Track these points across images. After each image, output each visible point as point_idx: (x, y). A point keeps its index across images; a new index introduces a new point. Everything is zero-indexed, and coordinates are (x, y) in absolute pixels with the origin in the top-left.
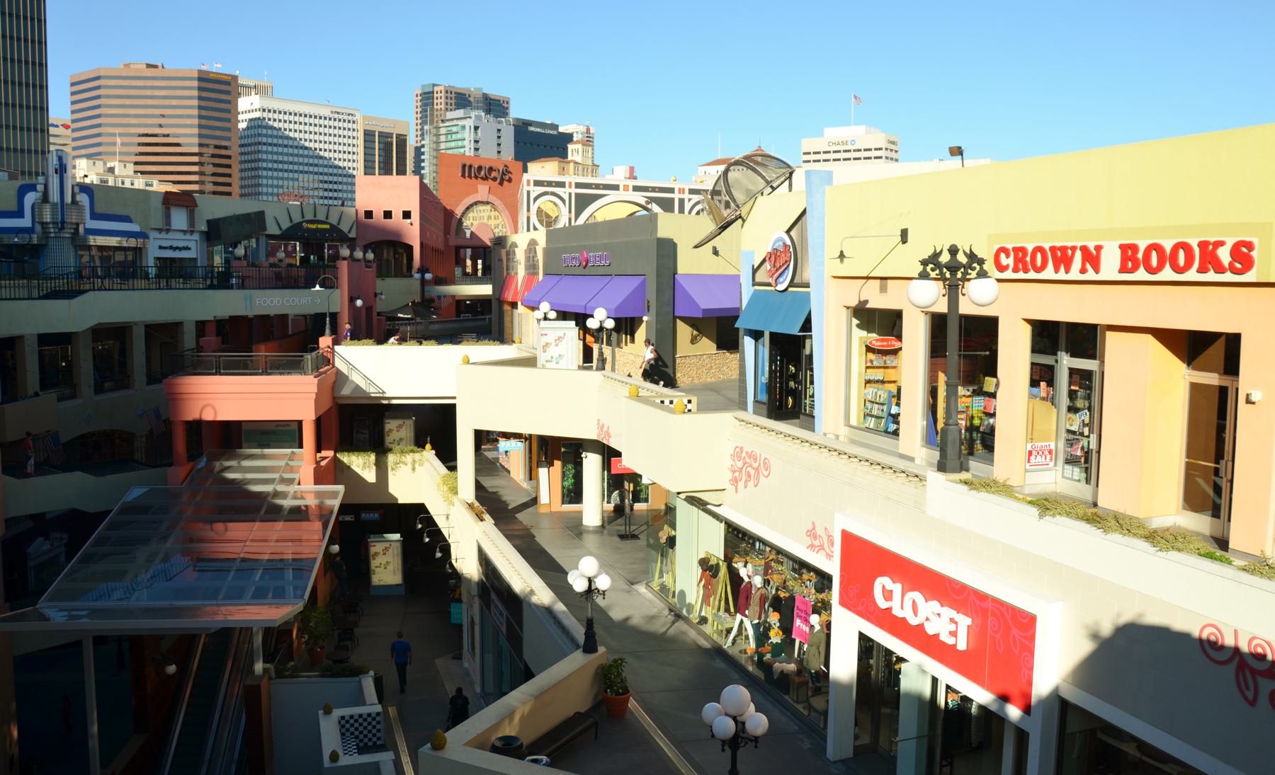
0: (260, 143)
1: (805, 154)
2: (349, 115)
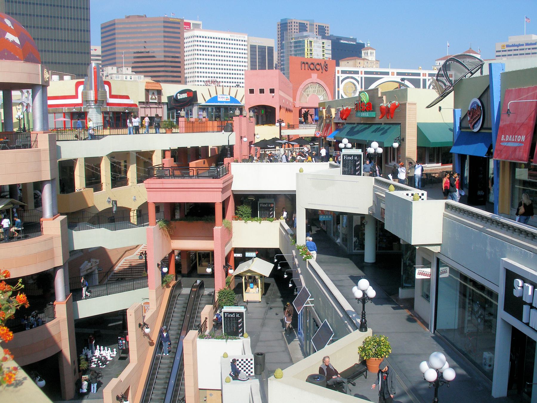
1: (497, 51)
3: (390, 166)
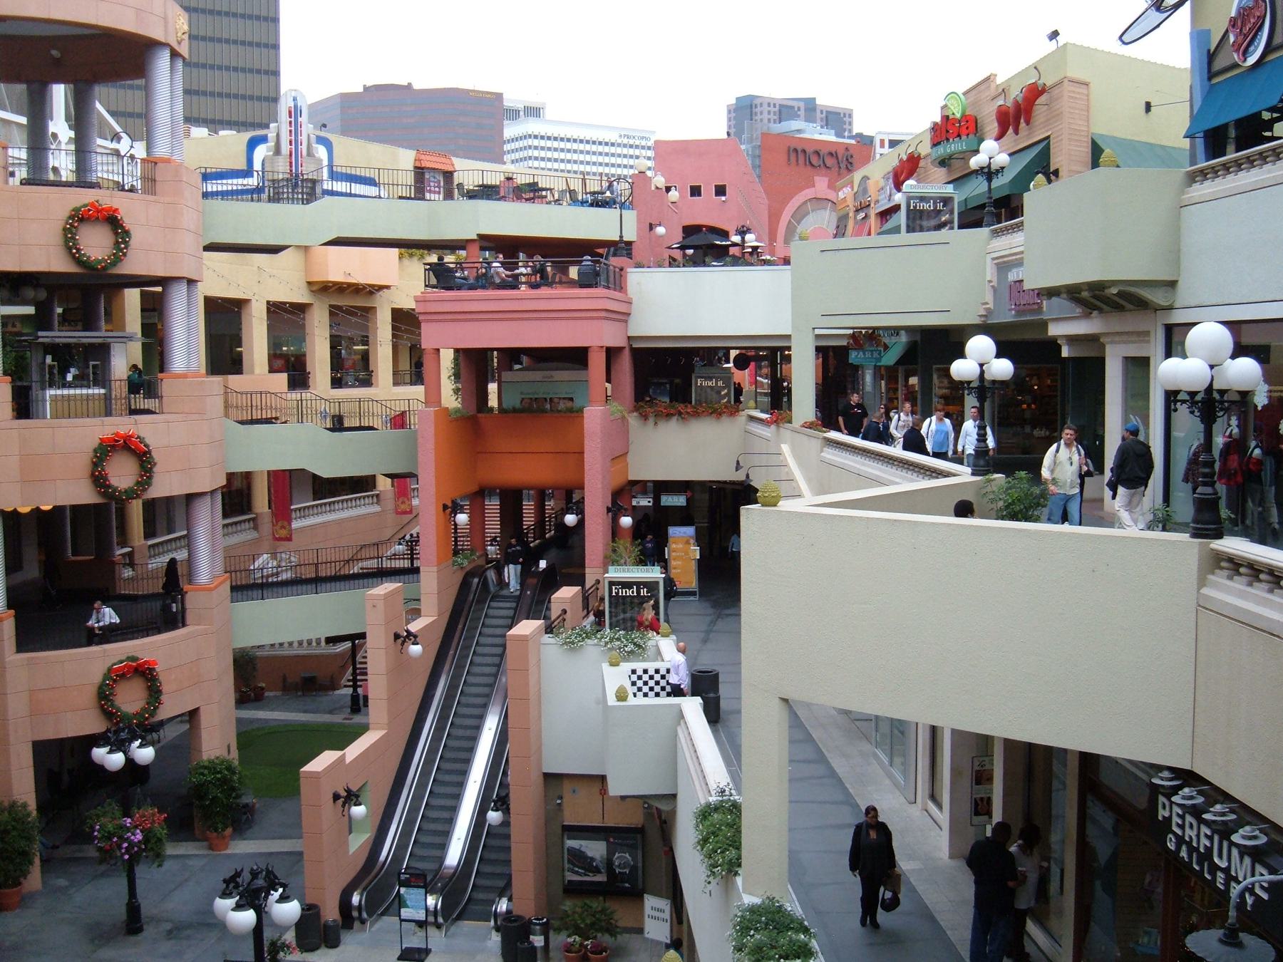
0: (530, 158)
2: (643, 138)
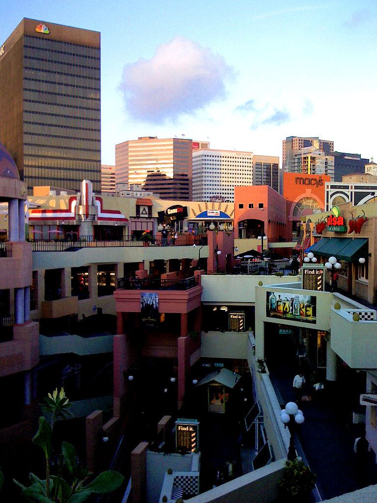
3: (359, 282)
